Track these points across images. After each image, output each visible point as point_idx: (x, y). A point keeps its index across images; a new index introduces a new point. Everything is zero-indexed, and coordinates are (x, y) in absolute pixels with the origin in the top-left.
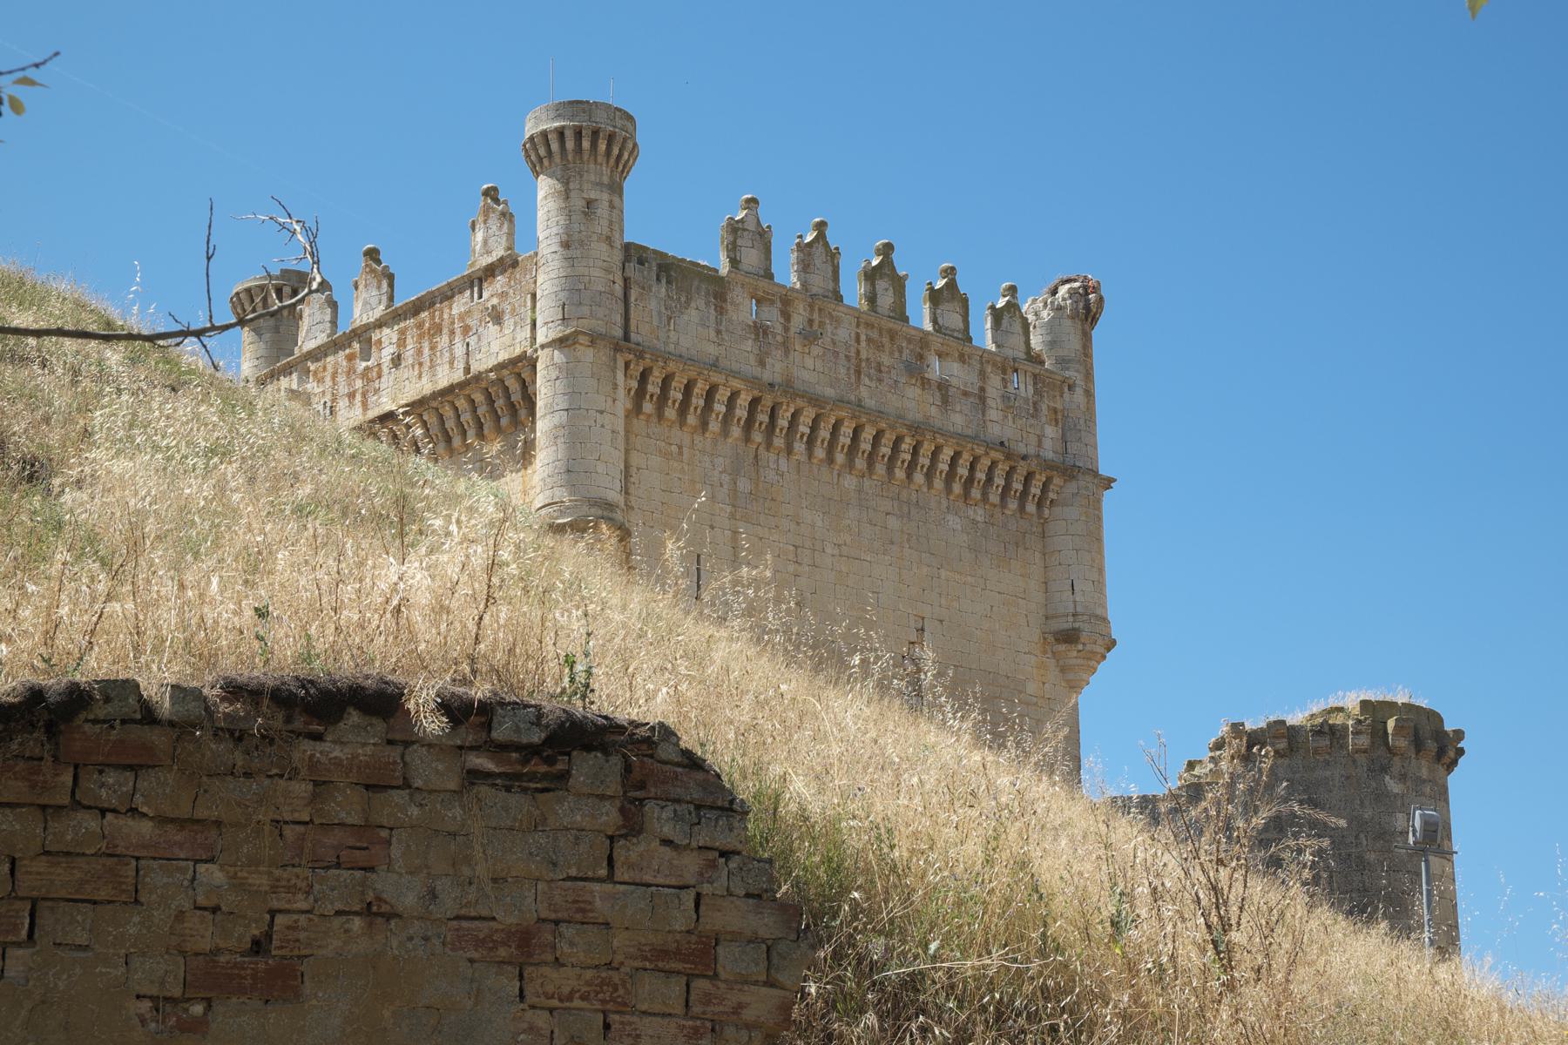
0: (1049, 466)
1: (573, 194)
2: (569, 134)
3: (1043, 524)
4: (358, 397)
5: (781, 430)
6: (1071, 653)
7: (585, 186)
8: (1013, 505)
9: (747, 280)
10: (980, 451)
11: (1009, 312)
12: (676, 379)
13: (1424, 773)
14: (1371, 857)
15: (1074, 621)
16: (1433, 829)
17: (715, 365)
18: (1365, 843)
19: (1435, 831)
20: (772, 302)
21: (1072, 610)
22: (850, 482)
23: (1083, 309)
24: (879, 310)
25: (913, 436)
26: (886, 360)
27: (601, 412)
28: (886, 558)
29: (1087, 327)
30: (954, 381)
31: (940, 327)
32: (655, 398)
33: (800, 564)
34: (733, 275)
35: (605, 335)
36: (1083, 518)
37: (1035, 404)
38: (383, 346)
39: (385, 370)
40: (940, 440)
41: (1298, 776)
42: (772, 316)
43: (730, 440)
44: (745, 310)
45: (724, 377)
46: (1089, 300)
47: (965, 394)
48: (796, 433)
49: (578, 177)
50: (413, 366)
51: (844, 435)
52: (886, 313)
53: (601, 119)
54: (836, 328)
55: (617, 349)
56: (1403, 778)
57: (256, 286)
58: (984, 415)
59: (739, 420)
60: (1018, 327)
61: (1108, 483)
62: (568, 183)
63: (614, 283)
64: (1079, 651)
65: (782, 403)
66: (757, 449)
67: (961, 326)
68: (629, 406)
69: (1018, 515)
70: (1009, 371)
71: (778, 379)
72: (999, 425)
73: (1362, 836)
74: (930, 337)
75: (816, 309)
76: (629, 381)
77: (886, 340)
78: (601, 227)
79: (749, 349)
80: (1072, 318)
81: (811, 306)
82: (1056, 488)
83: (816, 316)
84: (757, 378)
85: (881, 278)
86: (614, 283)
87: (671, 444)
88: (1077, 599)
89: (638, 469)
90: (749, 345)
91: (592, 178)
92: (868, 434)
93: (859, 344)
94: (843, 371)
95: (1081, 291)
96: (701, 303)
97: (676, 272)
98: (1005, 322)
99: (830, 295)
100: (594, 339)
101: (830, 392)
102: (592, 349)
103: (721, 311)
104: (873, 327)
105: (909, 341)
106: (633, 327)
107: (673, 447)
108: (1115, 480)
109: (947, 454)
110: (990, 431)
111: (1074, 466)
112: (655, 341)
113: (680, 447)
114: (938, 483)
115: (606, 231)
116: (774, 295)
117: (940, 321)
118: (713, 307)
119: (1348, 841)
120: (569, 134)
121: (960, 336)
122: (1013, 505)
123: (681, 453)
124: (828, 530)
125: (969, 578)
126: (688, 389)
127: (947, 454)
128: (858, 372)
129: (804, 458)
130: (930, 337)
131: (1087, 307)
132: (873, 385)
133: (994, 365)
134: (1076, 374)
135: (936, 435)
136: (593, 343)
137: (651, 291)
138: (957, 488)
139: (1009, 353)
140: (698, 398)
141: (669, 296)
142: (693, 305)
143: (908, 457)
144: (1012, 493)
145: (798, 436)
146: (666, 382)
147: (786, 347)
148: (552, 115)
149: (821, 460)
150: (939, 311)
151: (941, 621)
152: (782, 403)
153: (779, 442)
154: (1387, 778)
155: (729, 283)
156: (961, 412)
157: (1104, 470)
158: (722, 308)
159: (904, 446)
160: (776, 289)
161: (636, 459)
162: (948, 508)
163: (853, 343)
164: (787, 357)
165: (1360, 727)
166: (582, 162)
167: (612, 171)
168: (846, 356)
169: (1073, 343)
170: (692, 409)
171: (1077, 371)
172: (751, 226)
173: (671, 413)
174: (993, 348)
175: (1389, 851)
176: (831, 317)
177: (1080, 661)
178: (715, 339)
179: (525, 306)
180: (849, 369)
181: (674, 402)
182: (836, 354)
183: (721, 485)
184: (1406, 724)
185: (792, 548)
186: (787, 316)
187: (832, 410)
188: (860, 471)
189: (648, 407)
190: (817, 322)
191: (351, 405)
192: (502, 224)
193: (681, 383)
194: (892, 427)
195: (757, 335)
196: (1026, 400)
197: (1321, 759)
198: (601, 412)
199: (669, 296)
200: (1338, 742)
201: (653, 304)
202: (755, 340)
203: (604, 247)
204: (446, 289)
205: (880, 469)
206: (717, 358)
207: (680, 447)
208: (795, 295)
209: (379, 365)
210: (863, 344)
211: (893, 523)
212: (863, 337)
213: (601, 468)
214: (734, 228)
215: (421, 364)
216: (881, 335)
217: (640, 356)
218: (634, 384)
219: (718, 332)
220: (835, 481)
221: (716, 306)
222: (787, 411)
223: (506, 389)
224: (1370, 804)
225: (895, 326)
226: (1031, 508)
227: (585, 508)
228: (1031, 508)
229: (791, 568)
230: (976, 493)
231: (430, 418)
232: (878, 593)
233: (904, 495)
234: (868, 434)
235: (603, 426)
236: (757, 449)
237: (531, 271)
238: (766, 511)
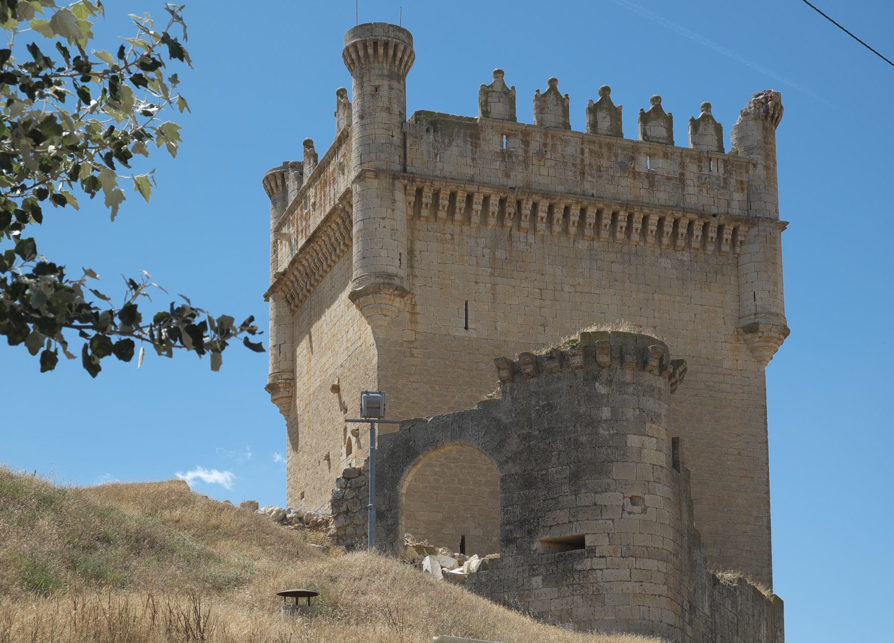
0: (737, 219)
1: (365, 84)
2: (359, 46)
3: (737, 258)
5: (526, 216)
6: (755, 338)
7: (372, 78)
8: (711, 248)
9: (495, 123)
10: (678, 215)
11: (704, 121)
12: (442, 192)
13: (628, 378)
14: (583, 439)
16: (376, 406)
17: (471, 181)
18: (580, 429)
19: (379, 408)
20: (516, 135)
21: (753, 311)
22: (582, 245)
23: (764, 112)
24: (599, 131)
25: (626, 210)
26: (604, 163)
27: (384, 218)
28: (611, 290)
29: (767, 124)
30: (659, 171)
31: (648, 137)
32: (429, 206)
33: (544, 300)
34: (484, 121)
35: (386, 170)
37: (724, 179)
40: (646, 211)
41: (542, 389)
42: (516, 144)
43: (490, 227)
44: (494, 142)
45: (476, 187)
46: (768, 106)
47: (668, 179)
51: (573, 215)
52: (605, 133)
54: (565, 147)
55: (395, 177)
56: (609, 383)
57: (270, 174)
58: (683, 191)
59: (493, 213)
60: (711, 130)
61: (784, 226)
62: (362, 78)
63: (393, 136)
64: (760, 337)
65: (523, 199)
66: (511, 230)
67: (665, 134)
68: (410, 212)
69: (717, 254)
70: (704, 160)
71: (520, 184)
72: (695, 196)
73: (578, 425)
74: (639, 145)
75: (550, 136)
76: (408, 197)
77: (605, 150)
78: (383, 102)
79: (497, 168)
80: (755, 119)
81: (546, 135)
82: (743, 233)
83: (549, 141)
84: (504, 185)
85: (601, 111)
86: (393, 136)
89: (421, 252)
91: (377, 72)
92: (591, 213)
93: (583, 155)
94: (570, 174)
95: (763, 101)
96: (460, 142)
97: (441, 125)
98: (701, 129)
99: (561, 126)
100: (377, 173)
101: (560, 188)
102: (377, 180)
103: (475, 145)
104: (594, 142)
105: (623, 149)
106: (409, 162)
107: (446, 236)
110: (688, 200)
111: (756, 217)
112: (425, 170)
113: (452, 235)
114: (651, 239)
115: (386, 104)
116: (516, 131)
117: (648, 133)
118: (469, 144)
119: (569, 429)
120: (359, 46)
121: (664, 141)
122: (711, 248)
123: (453, 239)
124: (566, 277)
125: (678, 298)
126: (453, 196)
128: (583, 174)
129: (547, 233)
130: (639, 145)
131: (767, 111)
132: (595, 180)
133: (692, 157)
134: (758, 156)
135: (643, 208)
136: (377, 176)
137: (422, 139)
138: (666, 240)
139: (704, 148)
140: (460, 202)
141: (436, 140)
142: (454, 144)
143: (624, 224)
144: (709, 239)
145: (539, 219)
146: (436, 195)
147: (526, 163)
148: (351, 36)
149: (559, 233)
150: (647, 127)
151: (655, 327)
152: (523, 199)
153: (525, 224)
154: (597, 384)
155: (482, 127)
156: (665, 191)
157: (782, 218)
158: (476, 143)
160: (517, 127)
161: (418, 246)
162: (661, 255)
163: (579, 155)
164: (527, 169)
165: (574, 351)
166: (370, 63)
167: (391, 66)
168: (573, 164)
169: (756, 134)
170: (457, 210)
171: (759, 154)
172: (498, 88)
173: (442, 214)
174: (691, 146)
175: (597, 434)
176: (561, 140)
177: (761, 344)
178: (472, 164)
180: (575, 172)
181: (444, 207)
182: (565, 164)
183: (484, 256)
184: (604, 346)
185: (537, 290)
186: (526, 143)
187: (561, 199)
188: (590, 237)
189: (425, 212)
190: (550, 145)
192: (344, 111)
193: (447, 194)
194: (609, 206)
195: (504, 158)
196: (718, 178)
197: (556, 376)
198: (384, 218)
199: (436, 140)
200: (566, 363)
202: (502, 161)
203: (385, 115)
205: (605, 234)
206: (473, 176)
207: (452, 235)
208: (532, 129)
210: (587, 155)
211: (616, 267)
212: (586, 151)
213: (383, 253)
214: (486, 91)
216: (601, 147)
217: (413, 181)
218: (413, 199)
219: (474, 159)
220: (572, 245)
221: (472, 143)
222: (527, 204)
224: (585, 403)
225: (612, 141)
226: (725, 248)
227: (373, 280)
228: (725, 248)
229: (537, 303)
230: (681, 242)
231: (325, 238)
233: (626, 249)
234: (591, 213)
235: (384, 227)
236: (511, 230)
238: (518, 269)
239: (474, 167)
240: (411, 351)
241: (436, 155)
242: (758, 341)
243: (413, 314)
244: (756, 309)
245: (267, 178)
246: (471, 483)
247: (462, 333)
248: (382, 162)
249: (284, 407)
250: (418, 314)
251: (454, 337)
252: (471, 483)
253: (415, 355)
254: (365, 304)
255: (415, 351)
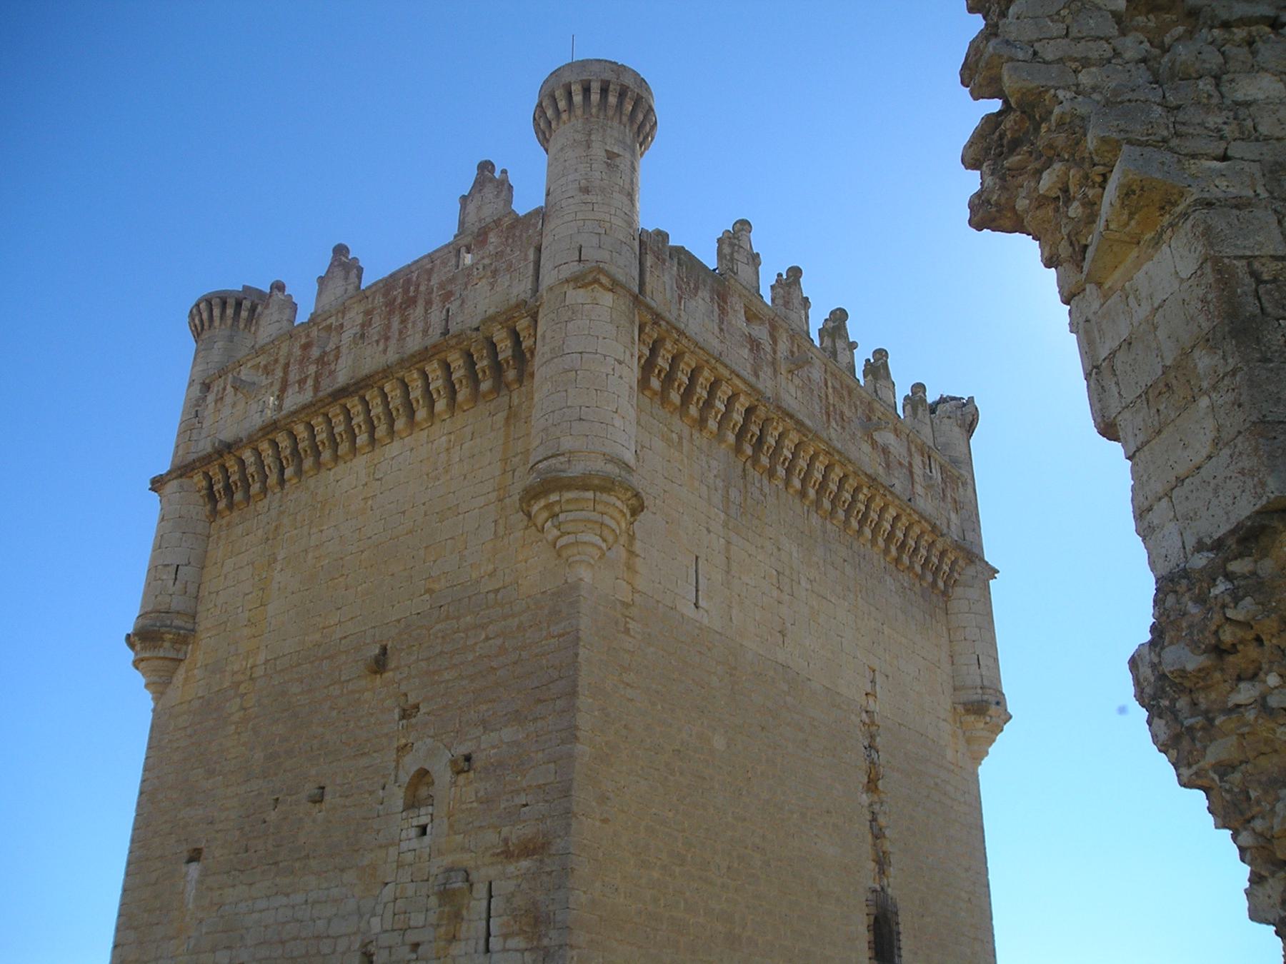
3: (946, 602)
4: (310, 382)
15: (983, 694)
27: (620, 363)
36: (983, 600)
38: (345, 329)
39: (344, 350)
42: (761, 332)
48: (781, 455)
49: (601, 130)
50: (377, 342)
53: (628, 81)
62: (590, 135)
85: (840, 338)
87: (672, 431)
88: (984, 673)
90: (745, 352)
96: (707, 295)
108: (998, 572)
109: (892, 512)
113: (680, 438)
127: (892, 512)
151: (887, 676)
159: (861, 497)
178: (719, 335)
179: (526, 260)
185: (775, 573)
191: (301, 390)
195: (752, 346)
198: (620, 363)
201: (666, 278)
202: (750, 349)
204: (426, 261)
209: (338, 348)
213: (618, 422)
215: (387, 339)
223: (493, 346)
232: (842, 637)
235: (621, 377)
237: (535, 225)
238: (754, 528)
239: (722, 342)
240: (627, 622)
241: (680, 298)
242: (982, 729)
243: (631, 553)
244: (982, 680)
245: (208, 300)
246: (702, 912)
247: (690, 611)
248: (619, 270)
249: (160, 677)
250: (637, 556)
251: (682, 616)
252: (702, 912)
253: (632, 633)
254: (570, 507)
255: (632, 625)
